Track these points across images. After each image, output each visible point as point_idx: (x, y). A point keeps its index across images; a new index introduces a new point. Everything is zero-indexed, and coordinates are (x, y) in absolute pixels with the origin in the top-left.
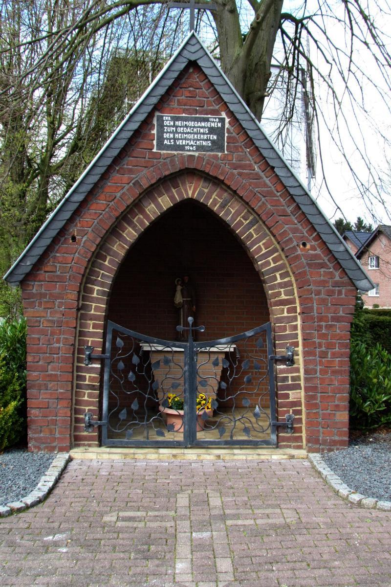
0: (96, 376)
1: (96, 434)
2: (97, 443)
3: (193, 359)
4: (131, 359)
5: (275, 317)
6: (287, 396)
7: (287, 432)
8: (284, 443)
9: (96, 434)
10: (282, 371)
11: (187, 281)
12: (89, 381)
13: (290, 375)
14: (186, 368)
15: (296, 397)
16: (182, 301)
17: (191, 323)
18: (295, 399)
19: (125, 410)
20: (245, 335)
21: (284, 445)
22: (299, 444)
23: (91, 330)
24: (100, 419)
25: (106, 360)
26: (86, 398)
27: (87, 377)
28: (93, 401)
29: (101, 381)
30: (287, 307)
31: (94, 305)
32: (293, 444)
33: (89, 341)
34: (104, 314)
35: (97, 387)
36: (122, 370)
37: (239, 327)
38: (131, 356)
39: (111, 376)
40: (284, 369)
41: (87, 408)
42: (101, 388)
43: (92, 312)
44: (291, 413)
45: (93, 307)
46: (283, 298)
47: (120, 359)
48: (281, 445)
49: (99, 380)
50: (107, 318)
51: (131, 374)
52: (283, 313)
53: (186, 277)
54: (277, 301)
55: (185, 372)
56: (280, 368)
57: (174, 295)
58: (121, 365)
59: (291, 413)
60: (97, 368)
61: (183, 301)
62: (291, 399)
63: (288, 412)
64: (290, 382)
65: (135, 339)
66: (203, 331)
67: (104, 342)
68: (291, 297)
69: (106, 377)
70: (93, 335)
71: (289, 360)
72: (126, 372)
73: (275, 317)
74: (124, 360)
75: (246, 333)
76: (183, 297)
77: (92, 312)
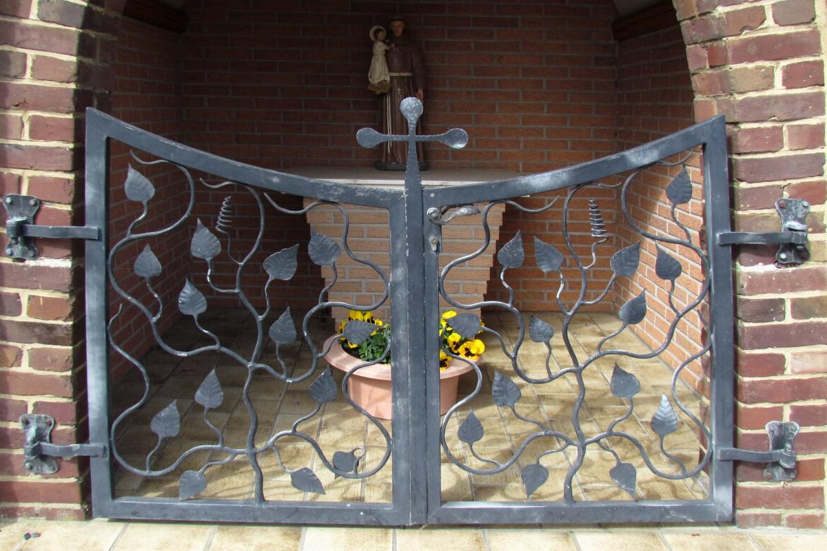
0: (58, 295)
1: (73, 480)
2: (77, 506)
3: (424, 245)
4: (187, 245)
5: (740, 98)
6: (777, 364)
7: (771, 479)
8: (758, 511)
9: (73, 480)
10: (759, 284)
11: (399, 32)
12: (30, 314)
13: (788, 297)
14: (400, 273)
15: (809, 366)
16: (388, 79)
17: (412, 119)
18: (803, 373)
19: (213, 371)
20: (623, 158)
21: (756, 516)
22: (809, 512)
23: (26, 141)
24: (82, 434)
25: (89, 246)
26: (25, 367)
27: (24, 301)
28: (52, 379)
29: (78, 311)
30: (784, 63)
31: (31, 54)
32: (786, 513)
33: (20, 179)
34: (73, 86)
35: (60, 333)
36: (154, 280)
37: (532, 138)
38: (187, 230)
39: (110, 297)
40: (768, 276)
41: (31, 400)
42: (78, 334)
43: (27, 80)
44: (786, 418)
45: (29, 63)
46: (771, 32)
47: (142, 243)
48: (745, 517)
49: (69, 310)
50: (81, 101)
51: (188, 290)
52: (770, 85)
53: (397, 23)
54: (747, 43)
55: (395, 286)
56: (754, 275)
57: (366, 67)
58: (149, 263)
59: (786, 418)
60: (57, 270)
61: (391, 78)
62: (788, 375)
63: (777, 414)
64: (789, 320)
65: (195, 173)
66: (460, 146)
67: (79, 185)
68: (803, 29)
69: (93, 302)
70: (37, 158)
71: (790, 247)
72: (169, 284)
73: (740, 98)
74: (158, 246)
75: (627, 153)
76: (390, 70)
77: (27, 80)
